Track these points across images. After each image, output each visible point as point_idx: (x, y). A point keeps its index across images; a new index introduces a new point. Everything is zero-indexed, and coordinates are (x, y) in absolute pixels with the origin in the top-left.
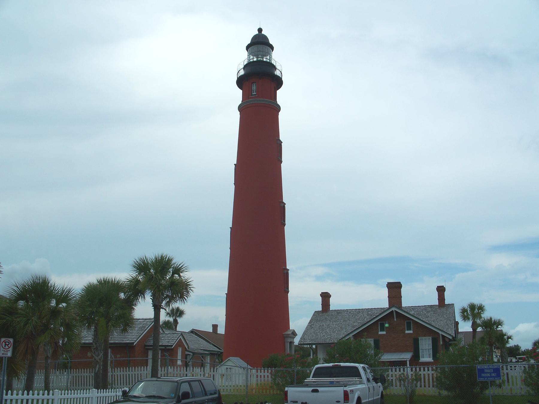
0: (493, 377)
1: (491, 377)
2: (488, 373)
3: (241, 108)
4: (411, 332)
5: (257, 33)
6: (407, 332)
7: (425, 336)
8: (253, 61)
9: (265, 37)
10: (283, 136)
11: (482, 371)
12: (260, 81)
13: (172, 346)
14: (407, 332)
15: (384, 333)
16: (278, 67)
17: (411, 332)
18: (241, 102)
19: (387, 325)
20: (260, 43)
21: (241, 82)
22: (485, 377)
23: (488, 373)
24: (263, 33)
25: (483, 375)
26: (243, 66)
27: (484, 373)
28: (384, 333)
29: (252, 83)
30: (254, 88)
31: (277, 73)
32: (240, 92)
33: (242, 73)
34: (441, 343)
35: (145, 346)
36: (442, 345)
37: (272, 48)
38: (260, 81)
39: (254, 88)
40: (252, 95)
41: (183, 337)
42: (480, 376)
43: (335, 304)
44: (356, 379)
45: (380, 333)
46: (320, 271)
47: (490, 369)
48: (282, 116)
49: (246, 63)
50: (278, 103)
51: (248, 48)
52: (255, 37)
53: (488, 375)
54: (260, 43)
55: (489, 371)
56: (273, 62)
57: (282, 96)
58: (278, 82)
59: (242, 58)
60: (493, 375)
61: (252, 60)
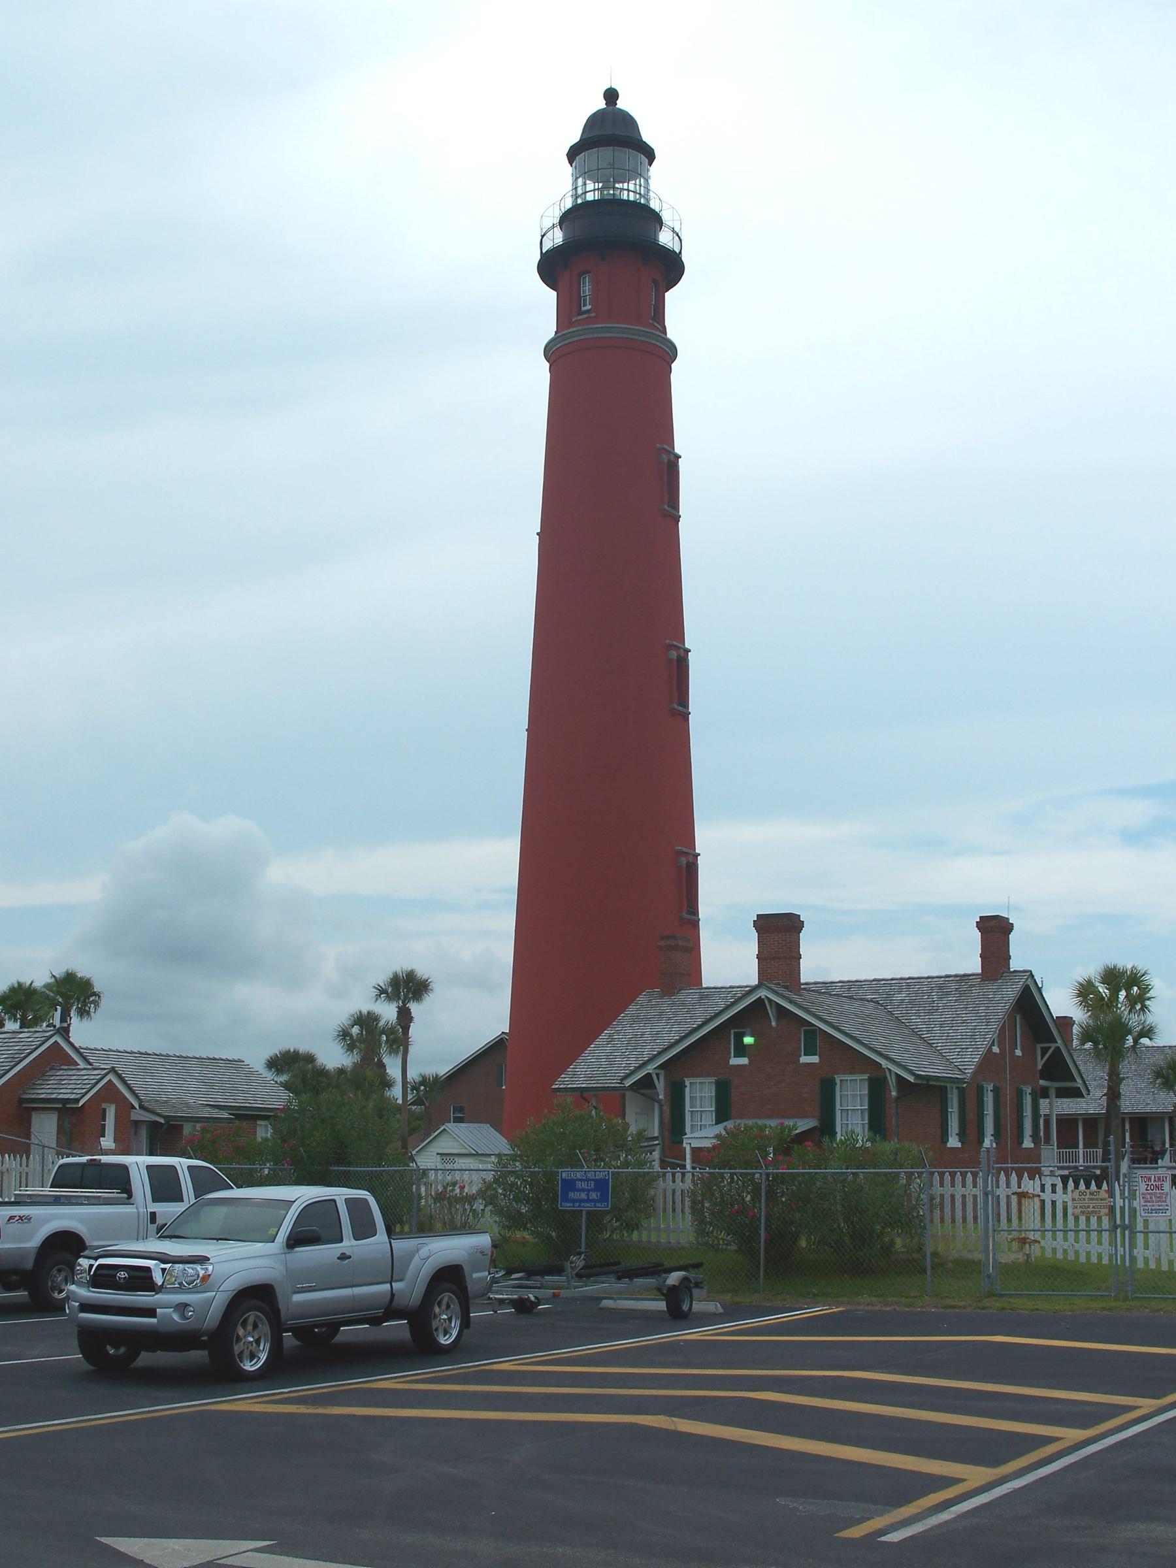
0: (593, 1201)
1: (588, 1200)
2: (583, 1190)
3: (552, 352)
4: (815, 1059)
5: (601, 104)
6: (804, 1059)
7: (852, 1072)
8: (587, 204)
9: (628, 122)
10: (686, 438)
11: (570, 1185)
12: (612, 261)
13: (77, 1100)
14: (804, 1059)
15: (744, 1061)
16: (666, 216)
17: (815, 1059)
18: (552, 335)
19: (748, 1040)
20: (611, 138)
21: (551, 267)
22: (574, 1201)
23: (583, 1190)
24: (621, 104)
25: (572, 1195)
26: (557, 221)
27: (575, 1189)
28: (744, 1061)
29: (580, 275)
30: (587, 289)
31: (665, 238)
32: (553, 294)
33: (557, 237)
34: (894, 1094)
35: (22, 1101)
36: (897, 1098)
37: (650, 155)
38: (612, 261)
39: (587, 289)
40: (580, 313)
41: (119, 1076)
42: (565, 1198)
43: (818, 961)
44: (114, 1194)
45: (734, 1061)
46: (1137, 812)
47: (588, 1180)
48: (680, 375)
49: (569, 204)
50: (670, 335)
51: (573, 154)
52: (594, 121)
53: (583, 1196)
54: (611, 138)
55: (584, 1185)
56: (654, 205)
57: (682, 311)
58: (670, 268)
59: (545, 191)
60: (594, 1196)
61: (579, 201)
